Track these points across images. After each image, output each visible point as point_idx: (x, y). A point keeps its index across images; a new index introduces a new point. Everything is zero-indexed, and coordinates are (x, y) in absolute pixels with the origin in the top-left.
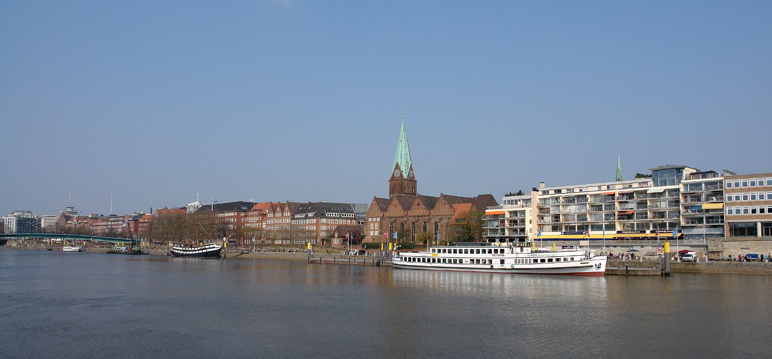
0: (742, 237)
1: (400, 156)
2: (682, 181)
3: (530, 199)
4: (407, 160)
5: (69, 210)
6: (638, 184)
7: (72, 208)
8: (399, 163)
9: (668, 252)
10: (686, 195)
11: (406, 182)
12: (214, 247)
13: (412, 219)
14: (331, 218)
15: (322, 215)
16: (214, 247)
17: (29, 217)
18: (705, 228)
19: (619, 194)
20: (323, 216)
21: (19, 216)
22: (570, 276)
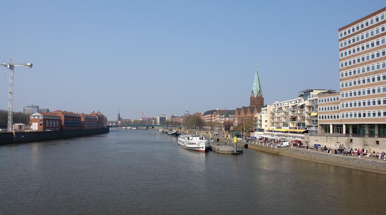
0: (303, 134)
1: (254, 86)
2: (308, 99)
3: (267, 109)
4: (257, 88)
5: (187, 113)
6: (13, 125)
7: (188, 112)
8: (253, 90)
9: (235, 142)
10: (310, 107)
11: (256, 99)
12: (174, 131)
13: (247, 118)
14: (231, 117)
15: (227, 116)
16: (174, 131)
17: (164, 117)
18: (315, 127)
19: (291, 106)
20: (228, 116)
21: (161, 116)
22: (195, 151)
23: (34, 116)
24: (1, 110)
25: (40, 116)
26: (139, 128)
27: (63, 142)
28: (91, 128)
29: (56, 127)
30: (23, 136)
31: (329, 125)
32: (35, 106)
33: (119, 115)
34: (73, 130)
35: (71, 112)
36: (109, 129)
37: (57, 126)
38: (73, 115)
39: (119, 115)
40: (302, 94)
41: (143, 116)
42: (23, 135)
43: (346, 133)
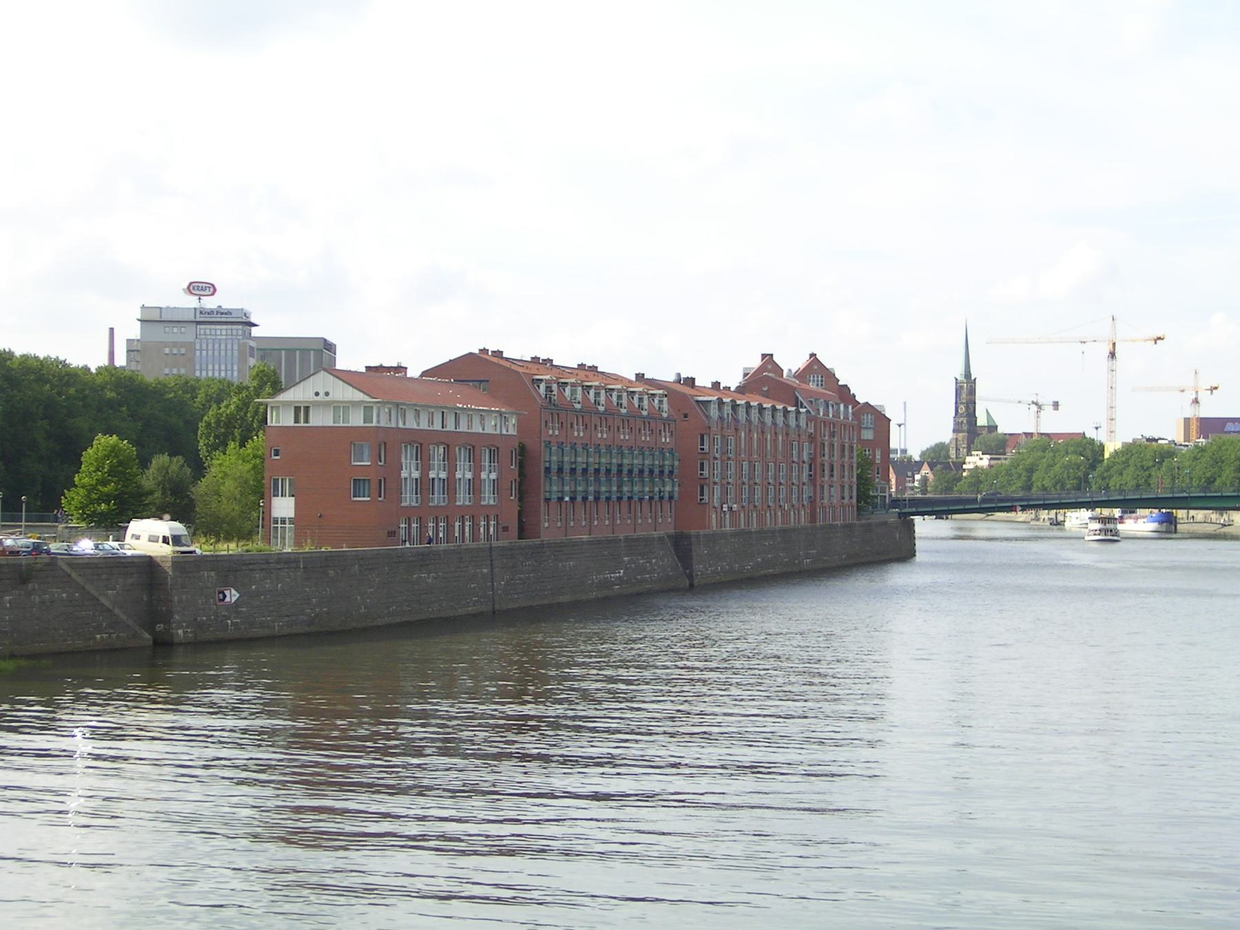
23: (302, 411)
24: (10, 355)
25: (355, 404)
26: (1193, 518)
27: (860, 582)
28: (761, 519)
29: (474, 513)
30: (232, 596)
31: (300, 407)
32: (229, 312)
33: (966, 393)
34: (616, 541)
35: (543, 356)
36: (911, 525)
37: (489, 499)
38: (630, 403)
39: (966, 393)
40: (1121, 525)
41: (161, 317)
42: (228, 585)
43: (1201, 418)
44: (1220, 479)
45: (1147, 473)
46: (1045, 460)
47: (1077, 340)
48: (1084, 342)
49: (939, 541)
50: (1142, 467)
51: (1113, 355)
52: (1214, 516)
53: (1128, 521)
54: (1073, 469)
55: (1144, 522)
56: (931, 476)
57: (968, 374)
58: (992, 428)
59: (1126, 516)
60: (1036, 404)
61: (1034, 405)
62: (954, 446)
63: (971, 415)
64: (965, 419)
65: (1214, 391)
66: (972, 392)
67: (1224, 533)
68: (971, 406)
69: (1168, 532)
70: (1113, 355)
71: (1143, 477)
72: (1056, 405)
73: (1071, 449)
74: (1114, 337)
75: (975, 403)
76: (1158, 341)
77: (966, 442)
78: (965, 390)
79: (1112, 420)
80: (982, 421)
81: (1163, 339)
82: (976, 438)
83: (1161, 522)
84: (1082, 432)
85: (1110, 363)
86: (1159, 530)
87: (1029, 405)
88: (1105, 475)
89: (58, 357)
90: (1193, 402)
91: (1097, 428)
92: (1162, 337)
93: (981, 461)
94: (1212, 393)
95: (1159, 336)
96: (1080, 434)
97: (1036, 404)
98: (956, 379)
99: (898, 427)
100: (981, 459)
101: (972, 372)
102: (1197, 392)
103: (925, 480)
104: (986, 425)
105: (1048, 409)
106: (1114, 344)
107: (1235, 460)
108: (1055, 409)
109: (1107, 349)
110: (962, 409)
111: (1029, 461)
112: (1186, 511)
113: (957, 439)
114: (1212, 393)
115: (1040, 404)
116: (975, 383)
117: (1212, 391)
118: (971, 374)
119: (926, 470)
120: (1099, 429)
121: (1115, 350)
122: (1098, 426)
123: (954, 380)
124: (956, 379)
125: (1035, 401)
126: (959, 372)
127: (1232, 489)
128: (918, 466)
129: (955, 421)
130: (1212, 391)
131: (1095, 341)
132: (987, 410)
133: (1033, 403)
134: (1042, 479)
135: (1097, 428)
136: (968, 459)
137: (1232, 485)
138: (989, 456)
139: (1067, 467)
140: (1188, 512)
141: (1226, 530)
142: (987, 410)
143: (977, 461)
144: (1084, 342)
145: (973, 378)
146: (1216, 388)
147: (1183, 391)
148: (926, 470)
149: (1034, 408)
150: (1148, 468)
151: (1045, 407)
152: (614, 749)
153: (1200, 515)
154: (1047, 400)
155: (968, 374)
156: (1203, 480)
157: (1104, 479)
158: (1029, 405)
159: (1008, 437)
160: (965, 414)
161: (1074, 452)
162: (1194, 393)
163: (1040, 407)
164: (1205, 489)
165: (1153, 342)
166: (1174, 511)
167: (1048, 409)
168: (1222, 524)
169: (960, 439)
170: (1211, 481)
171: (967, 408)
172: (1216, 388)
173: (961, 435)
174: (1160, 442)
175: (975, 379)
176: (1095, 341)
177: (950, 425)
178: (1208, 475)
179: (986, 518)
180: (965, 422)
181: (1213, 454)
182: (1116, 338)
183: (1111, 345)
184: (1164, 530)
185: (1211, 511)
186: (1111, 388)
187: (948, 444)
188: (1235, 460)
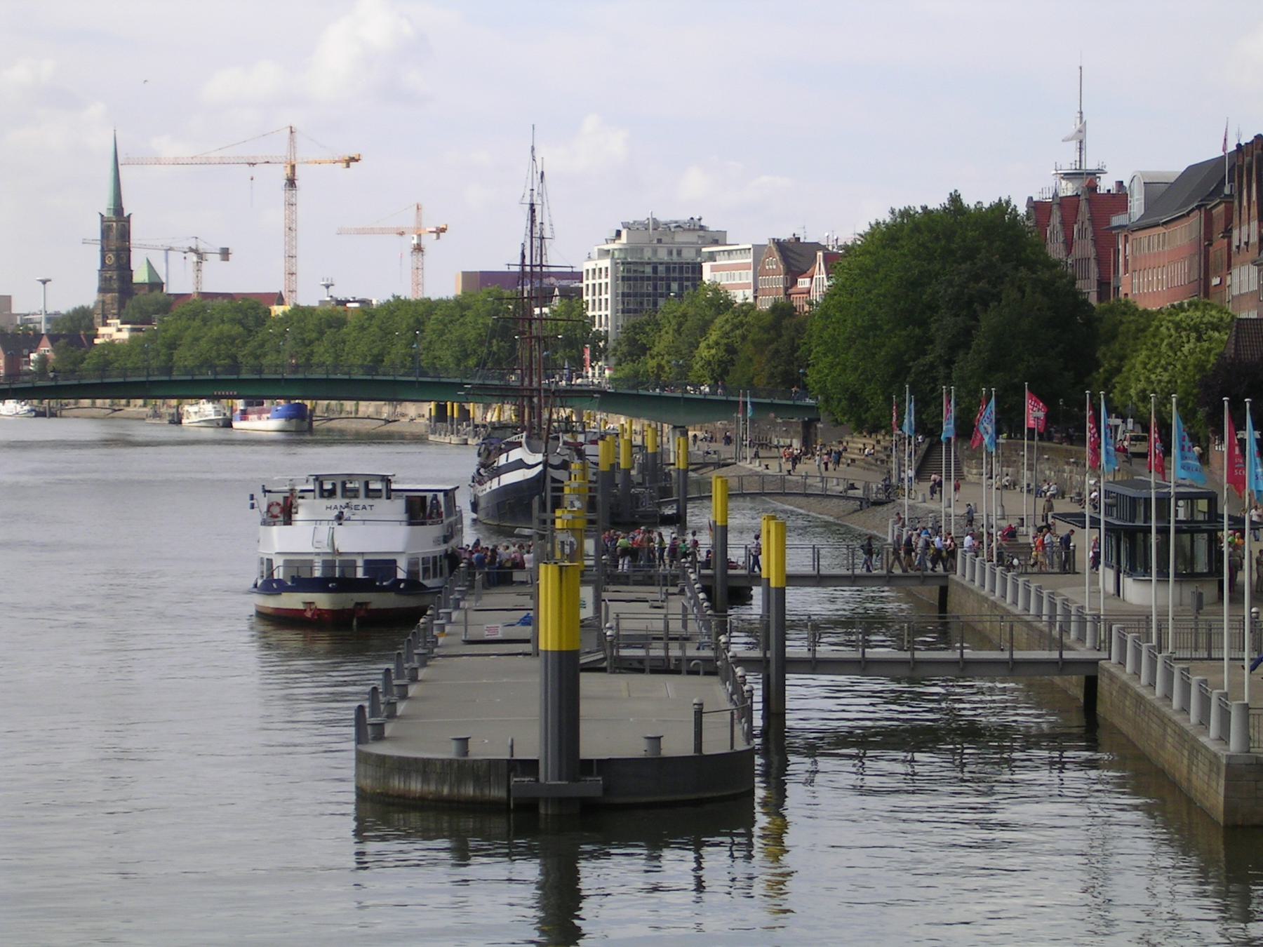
44: (388, 357)
45: (308, 350)
46: (190, 331)
47: (280, 160)
48: (254, 164)
49: (73, 454)
50: (303, 340)
51: (291, 183)
52: (386, 410)
53: (253, 417)
54: (225, 344)
55: (268, 418)
56: (51, 355)
57: (118, 209)
58: (156, 285)
59: (250, 409)
60: (196, 251)
61: (193, 254)
62: (100, 312)
63: (124, 267)
64: (115, 273)
65: (441, 234)
66: (125, 234)
67: (388, 431)
68: (123, 255)
69: (299, 432)
70: (291, 183)
71: (304, 355)
72: (225, 254)
73: (227, 316)
74: (293, 157)
75: (130, 251)
76: (351, 163)
77: (116, 306)
78: (114, 231)
79: (292, 274)
80: (140, 275)
81: (357, 161)
82: (128, 301)
83: (289, 418)
84: (277, 291)
85: (289, 193)
86: (288, 429)
87: (185, 252)
88: (259, 352)
89: (955, 199)
90: (415, 249)
91: (44, 282)
92: (357, 158)
93: (119, 333)
94: (438, 238)
95: (352, 156)
96: (277, 293)
97: (196, 251)
98: (102, 216)
99: (42, 286)
100: (119, 330)
101: (124, 206)
102: (419, 236)
103: (43, 360)
104: (147, 281)
105: (214, 260)
106: (293, 167)
107: (408, 331)
108: (223, 260)
109: (282, 173)
110: (111, 258)
111: (171, 332)
112: (355, 402)
113: (103, 302)
114: (438, 238)
115: (201, 251)
116: (129, 222)
117: (438, 234)
118: (122, 209)
119: (45, 348)
120: (331, 287)
121: (294, 175)
122: (329, 282)
123: (99, 216)
124: (102, 216)
125: (194, 247)
126: (104, 205)
127: (402, 371)
128: (33, 339)
129: (101, 276)
130: (438, 234)
131: (268, 162)
132: (148, 261)
133: (191, 250)
134: (185, 358)
135: (44, 282)
136: (102, 330)
137: (404, 366)
138: (129, 326)
139: (218, 341)
140: (357, 405)
141: (392, 427)
142: (148, 261)
143: (115, 332)
144: (254, 164)
145: (126, 214)
146: (443, 230)
147: (402, 234)
148: (45, 348)
149: (194, 258)
150: (311, 342)
151: (209, 256)
152: (811, 716)
153: (367, 408)
154: (211, 244)
155: (118, 209)
156: (369, 359)
157: (257, 357)
158: (185, 252)
159: (172, 298)
160: (115, 265)
161: (233, 321)
162: (415, 236)
163: (201, 256)
164: (371, 369)
165: (345, 165)
166: (308, 403)
167: (214, 260)
168: (385, 420)
169: (109, 301)
170: (378, 359)
171: (118, 257)
172: (443, 230)
173: (109, 295)
174: (349, 305)
175: (129, 216)
176: (268, 162)
177: (94, 282)
178: (375, 351)
179: (111, 415)
180: (115, 277)
181: (383, 323)
182: (295, 160)
183: (289, 168)
184: (293, 429)
185: (383, 403)
186: (290, 229)
187: (93, 309)
188: (408, 331)
